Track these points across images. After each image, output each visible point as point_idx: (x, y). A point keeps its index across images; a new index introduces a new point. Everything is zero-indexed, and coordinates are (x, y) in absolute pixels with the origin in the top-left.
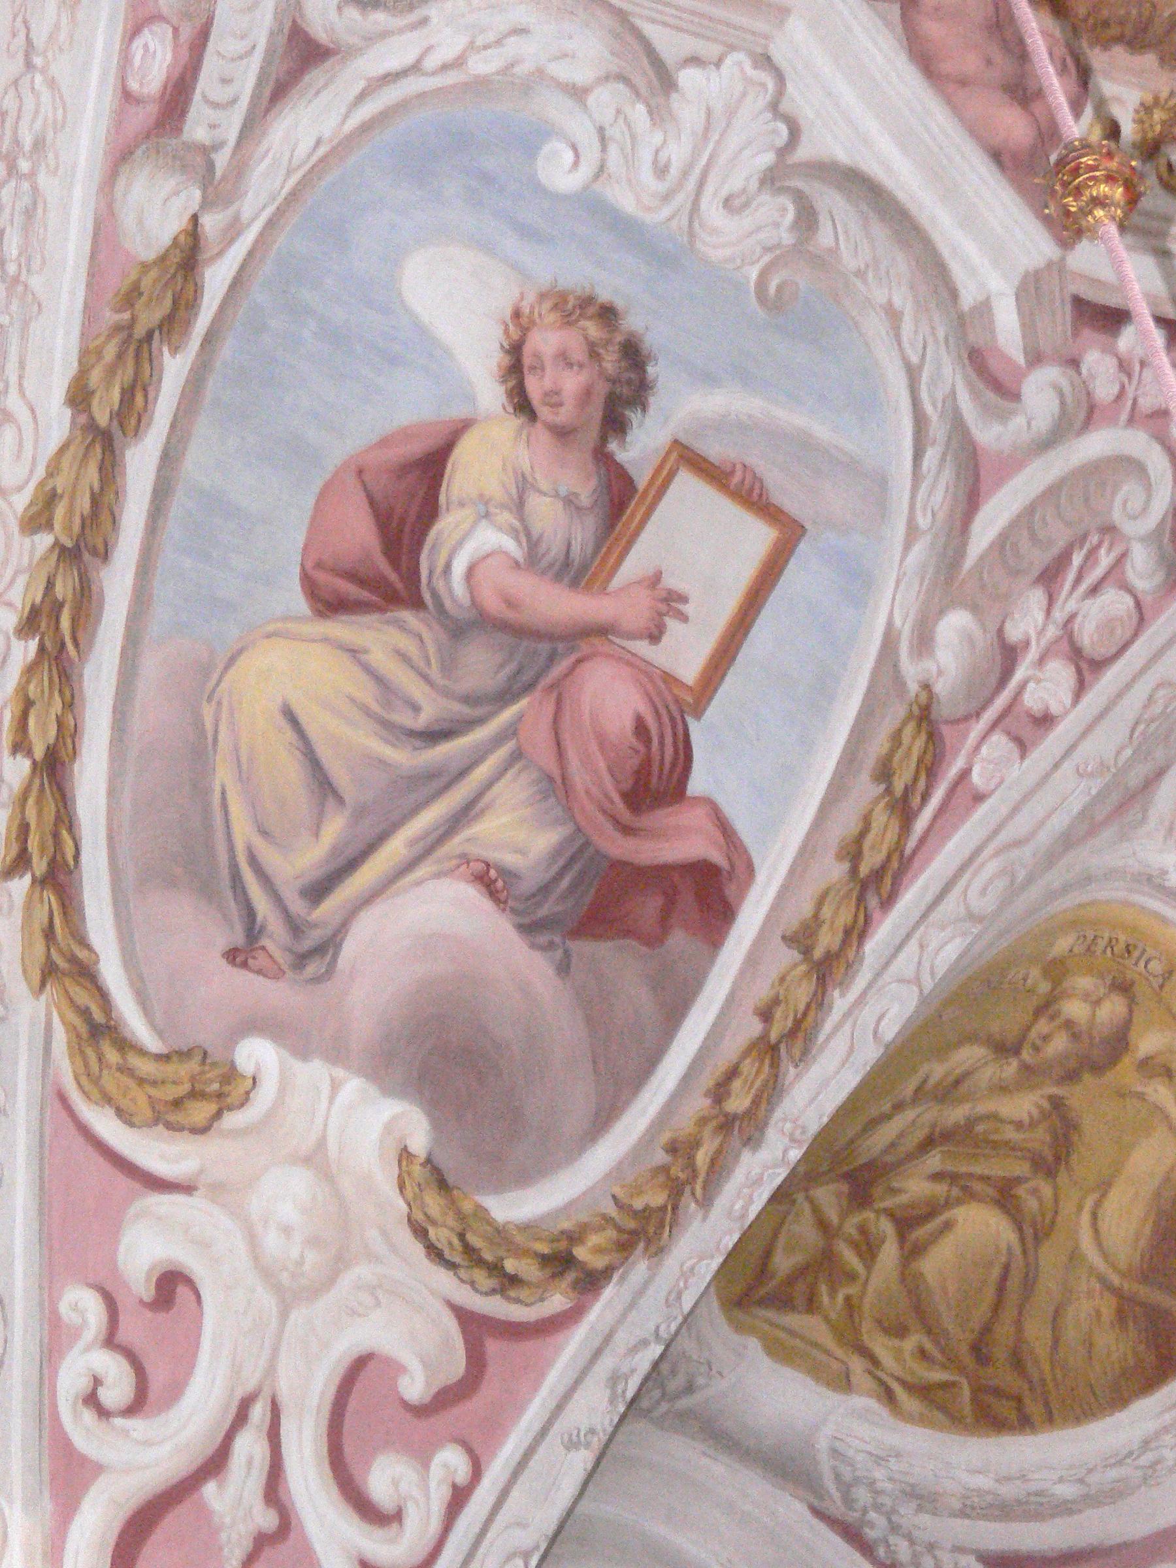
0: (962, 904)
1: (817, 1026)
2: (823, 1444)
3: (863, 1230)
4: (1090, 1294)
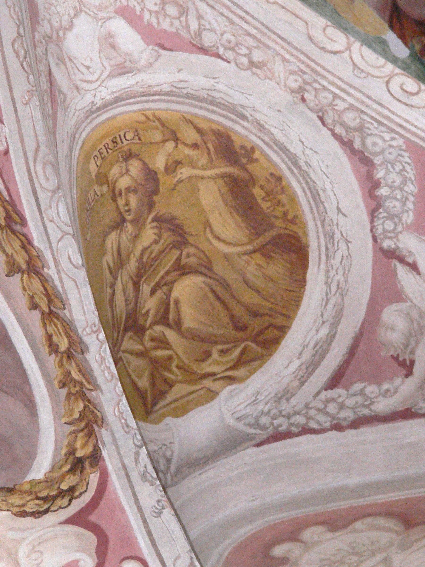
0: (46, 192)
1: (54, 288)
2: (232, 422)
3: (153, 339)
4: (248, 263)
